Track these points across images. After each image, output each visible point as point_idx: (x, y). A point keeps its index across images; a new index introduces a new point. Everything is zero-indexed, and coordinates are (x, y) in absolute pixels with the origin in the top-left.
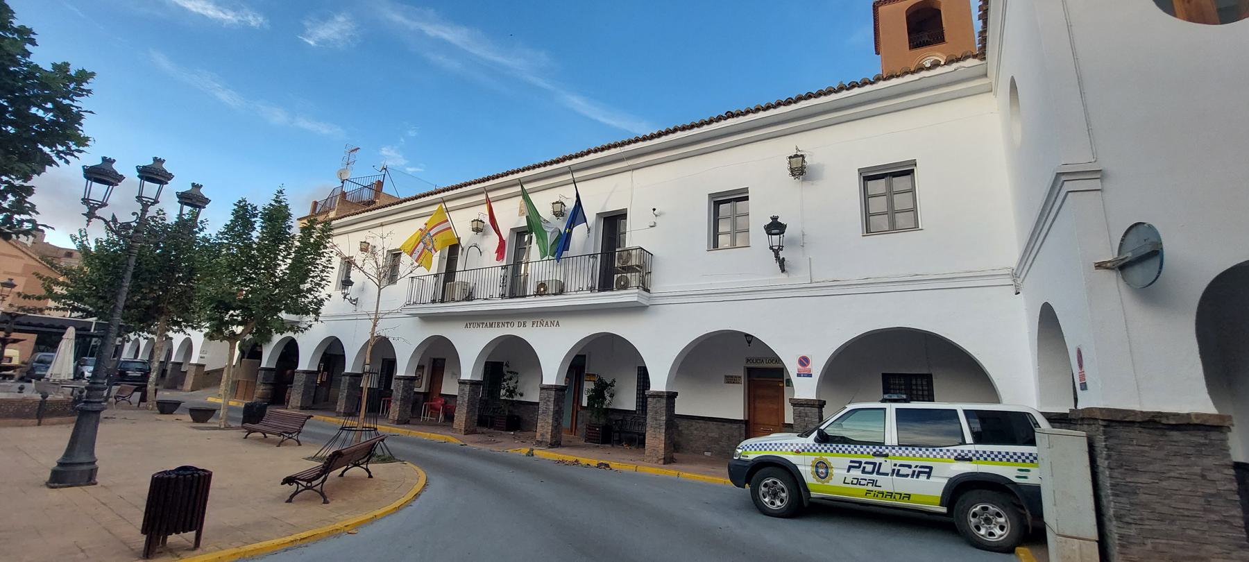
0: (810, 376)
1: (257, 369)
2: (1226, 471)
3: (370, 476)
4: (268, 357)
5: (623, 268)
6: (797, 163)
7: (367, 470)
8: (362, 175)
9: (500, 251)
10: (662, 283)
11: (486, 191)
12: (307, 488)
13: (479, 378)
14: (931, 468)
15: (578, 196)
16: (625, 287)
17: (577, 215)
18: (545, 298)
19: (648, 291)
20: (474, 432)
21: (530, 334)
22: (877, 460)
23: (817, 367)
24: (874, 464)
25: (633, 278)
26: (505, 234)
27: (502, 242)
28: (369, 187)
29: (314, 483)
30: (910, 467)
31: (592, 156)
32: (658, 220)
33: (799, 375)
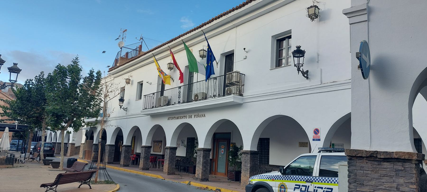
0: (319, 140)
1: (92, 144)
2: (411, 186)
3: (91, 188)
4: (96, 139)
5: (230, 84)
6: (312, 11)
7: (89, 185)
8: (131, 43)
9: (181, 78)
10: (249, 91)
11: (170, 49)
12: (51, 189)
13: (209, 147)
14: (332, 189)
15: (209, 45)
16: (230, 94)
17: (209, 56)
18: (197, 102)
19: (241, 95)
20: (173, 174)
21: (194, 122)
22: (308, 184)
23: (323, 135)
24: (306, 186)
25: (233, 89)
26: (183, 70)
27: (181, 74)
28: (136, 50)
29: (53, 187)
30: (322, 188)
31: (215, 22)
32: (248, 55)
33: (314, 140)
